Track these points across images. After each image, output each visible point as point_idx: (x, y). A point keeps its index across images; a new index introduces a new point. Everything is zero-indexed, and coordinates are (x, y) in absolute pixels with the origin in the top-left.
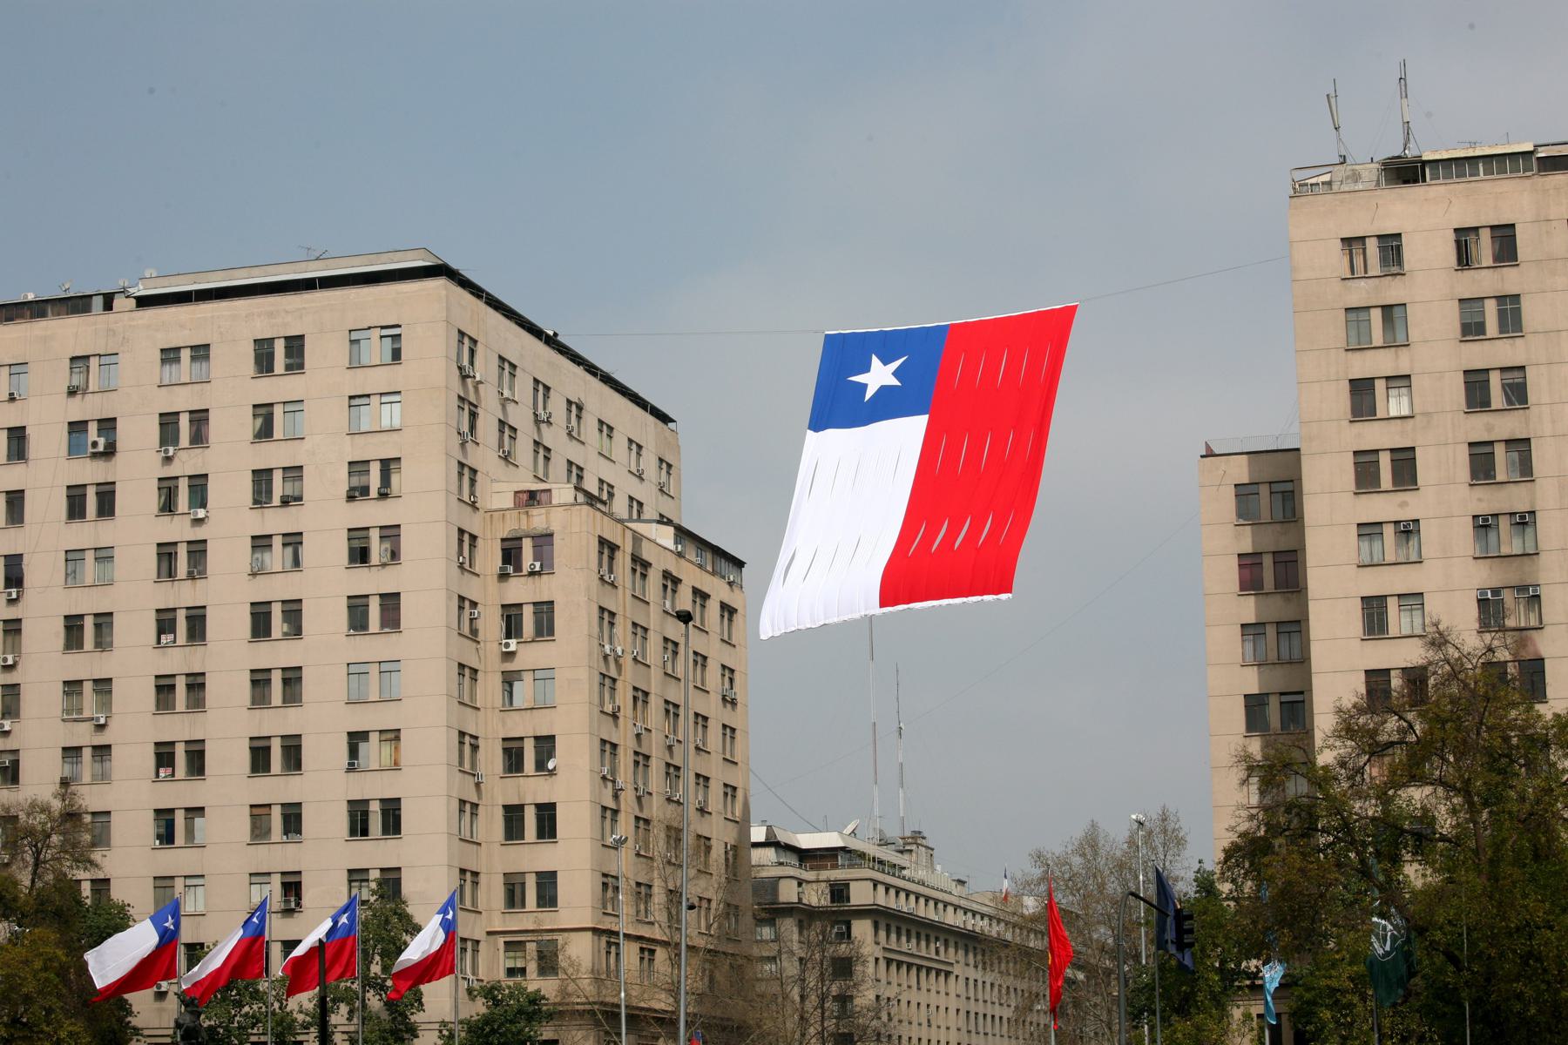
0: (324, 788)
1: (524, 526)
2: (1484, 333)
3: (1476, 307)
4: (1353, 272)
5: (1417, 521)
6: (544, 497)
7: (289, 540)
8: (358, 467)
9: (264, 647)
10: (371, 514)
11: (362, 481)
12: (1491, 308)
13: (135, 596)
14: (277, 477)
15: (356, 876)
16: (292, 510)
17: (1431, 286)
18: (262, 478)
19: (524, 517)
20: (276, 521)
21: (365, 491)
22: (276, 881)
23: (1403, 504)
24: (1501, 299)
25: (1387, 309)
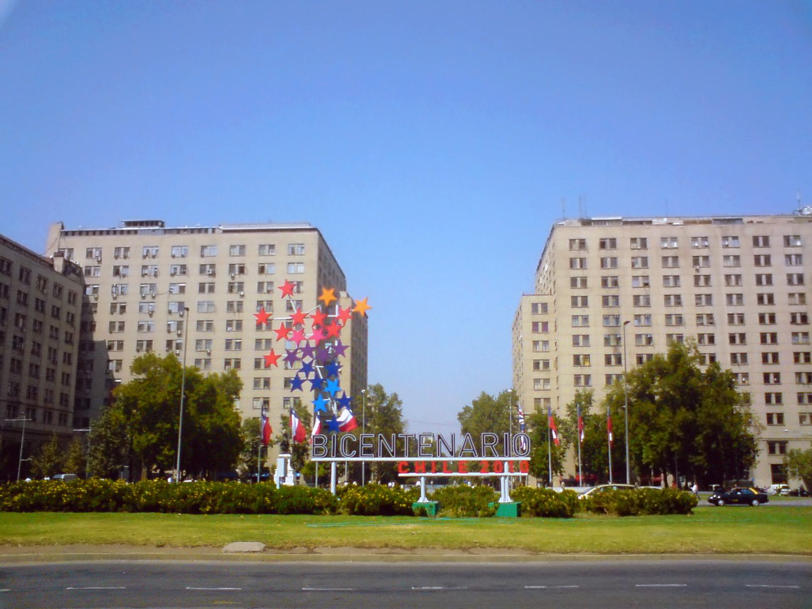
13: (220, 317)
14: (265, 285)
15: (669, 336)
17: (593, 254)
18: (261, 284)
24: (612, 258)
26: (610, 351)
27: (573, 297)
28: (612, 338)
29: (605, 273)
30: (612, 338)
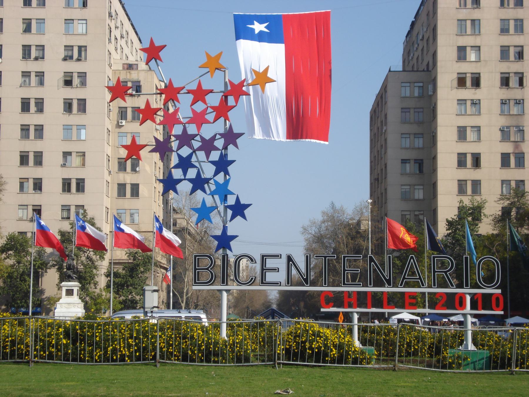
0: (52, 173)
1: (128, 77)
2: (509, 32)
3: (506, 22)
4: (460, 6)
5: (480, 100)
6: (135, 67)
7: (38, 74)
8: (69, 48)
9: (26, 116)
10: (74, 67)
11: (70, 53)
12: (512, 23)
14: (33, 49)
16: (40, 62)
19: (128, 74)
20: (32, 66)
21: (71, 57)
22: (30, 209)
23: (475, 94)
24: (516, 20)
25: (473, 21)
26: (508, 148)
27: (24, 46)
28: (513, 130)
29: (506, 40)
30: (513, 130)
